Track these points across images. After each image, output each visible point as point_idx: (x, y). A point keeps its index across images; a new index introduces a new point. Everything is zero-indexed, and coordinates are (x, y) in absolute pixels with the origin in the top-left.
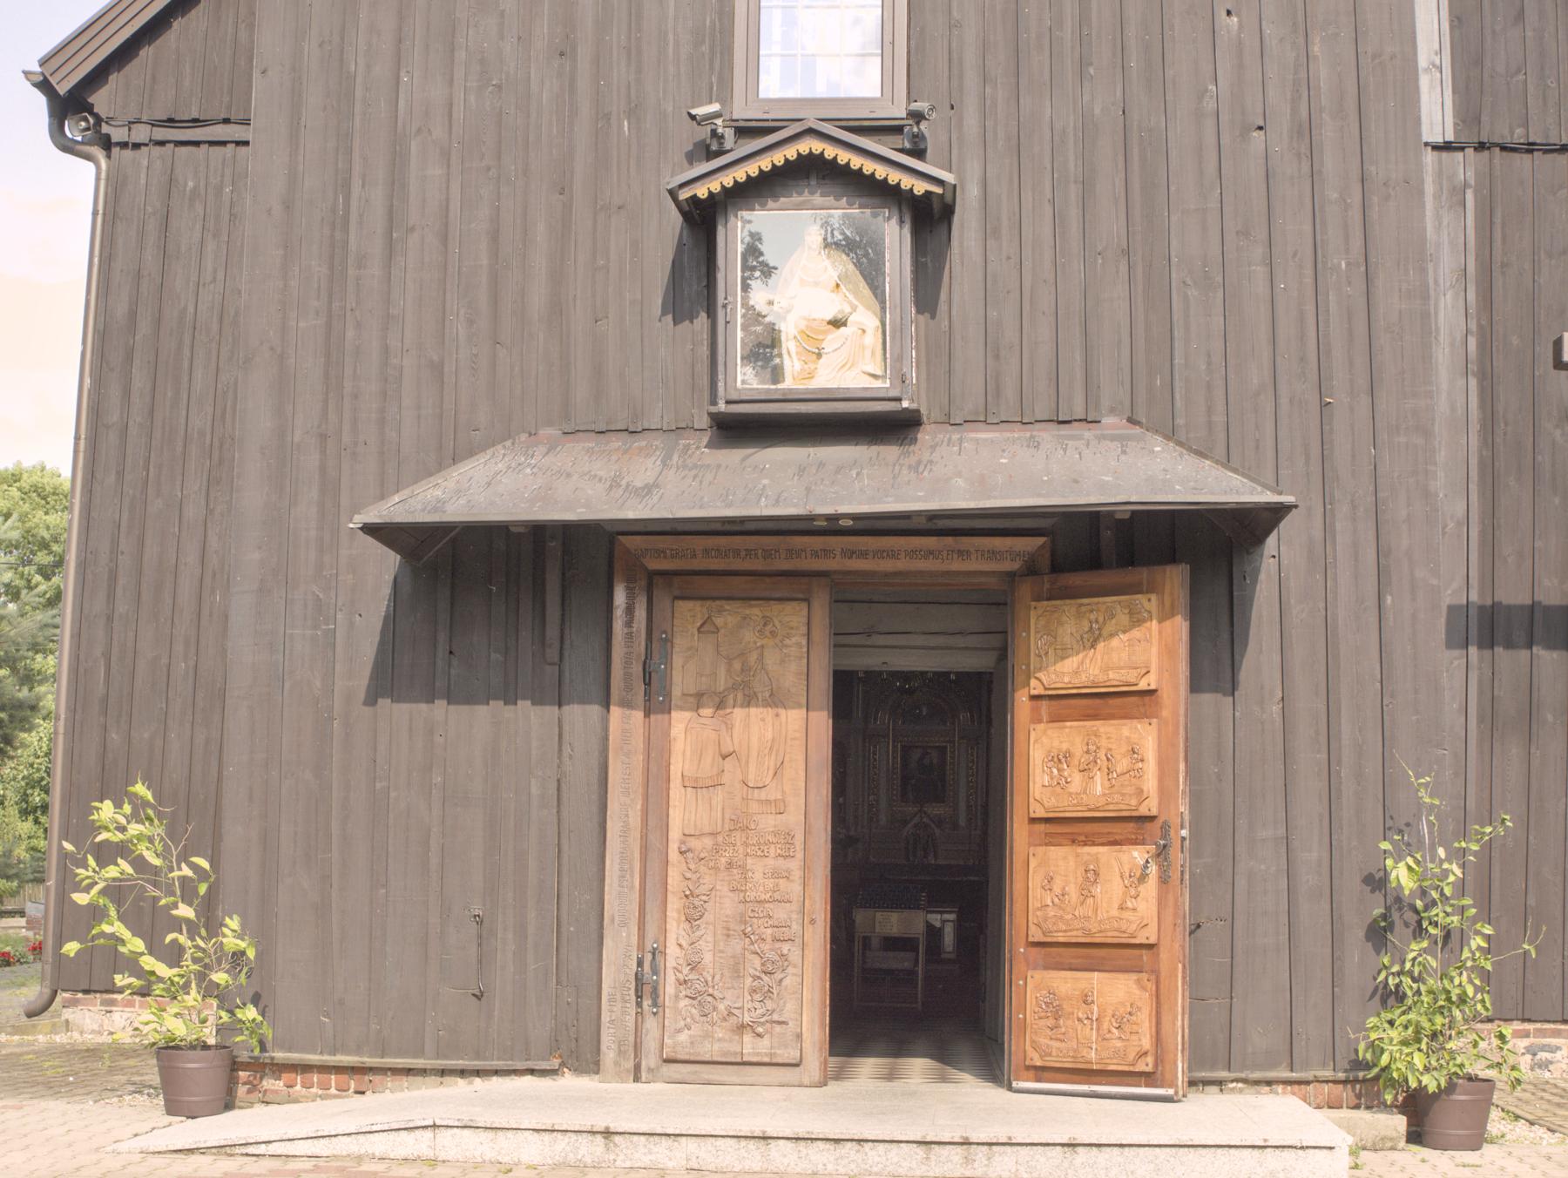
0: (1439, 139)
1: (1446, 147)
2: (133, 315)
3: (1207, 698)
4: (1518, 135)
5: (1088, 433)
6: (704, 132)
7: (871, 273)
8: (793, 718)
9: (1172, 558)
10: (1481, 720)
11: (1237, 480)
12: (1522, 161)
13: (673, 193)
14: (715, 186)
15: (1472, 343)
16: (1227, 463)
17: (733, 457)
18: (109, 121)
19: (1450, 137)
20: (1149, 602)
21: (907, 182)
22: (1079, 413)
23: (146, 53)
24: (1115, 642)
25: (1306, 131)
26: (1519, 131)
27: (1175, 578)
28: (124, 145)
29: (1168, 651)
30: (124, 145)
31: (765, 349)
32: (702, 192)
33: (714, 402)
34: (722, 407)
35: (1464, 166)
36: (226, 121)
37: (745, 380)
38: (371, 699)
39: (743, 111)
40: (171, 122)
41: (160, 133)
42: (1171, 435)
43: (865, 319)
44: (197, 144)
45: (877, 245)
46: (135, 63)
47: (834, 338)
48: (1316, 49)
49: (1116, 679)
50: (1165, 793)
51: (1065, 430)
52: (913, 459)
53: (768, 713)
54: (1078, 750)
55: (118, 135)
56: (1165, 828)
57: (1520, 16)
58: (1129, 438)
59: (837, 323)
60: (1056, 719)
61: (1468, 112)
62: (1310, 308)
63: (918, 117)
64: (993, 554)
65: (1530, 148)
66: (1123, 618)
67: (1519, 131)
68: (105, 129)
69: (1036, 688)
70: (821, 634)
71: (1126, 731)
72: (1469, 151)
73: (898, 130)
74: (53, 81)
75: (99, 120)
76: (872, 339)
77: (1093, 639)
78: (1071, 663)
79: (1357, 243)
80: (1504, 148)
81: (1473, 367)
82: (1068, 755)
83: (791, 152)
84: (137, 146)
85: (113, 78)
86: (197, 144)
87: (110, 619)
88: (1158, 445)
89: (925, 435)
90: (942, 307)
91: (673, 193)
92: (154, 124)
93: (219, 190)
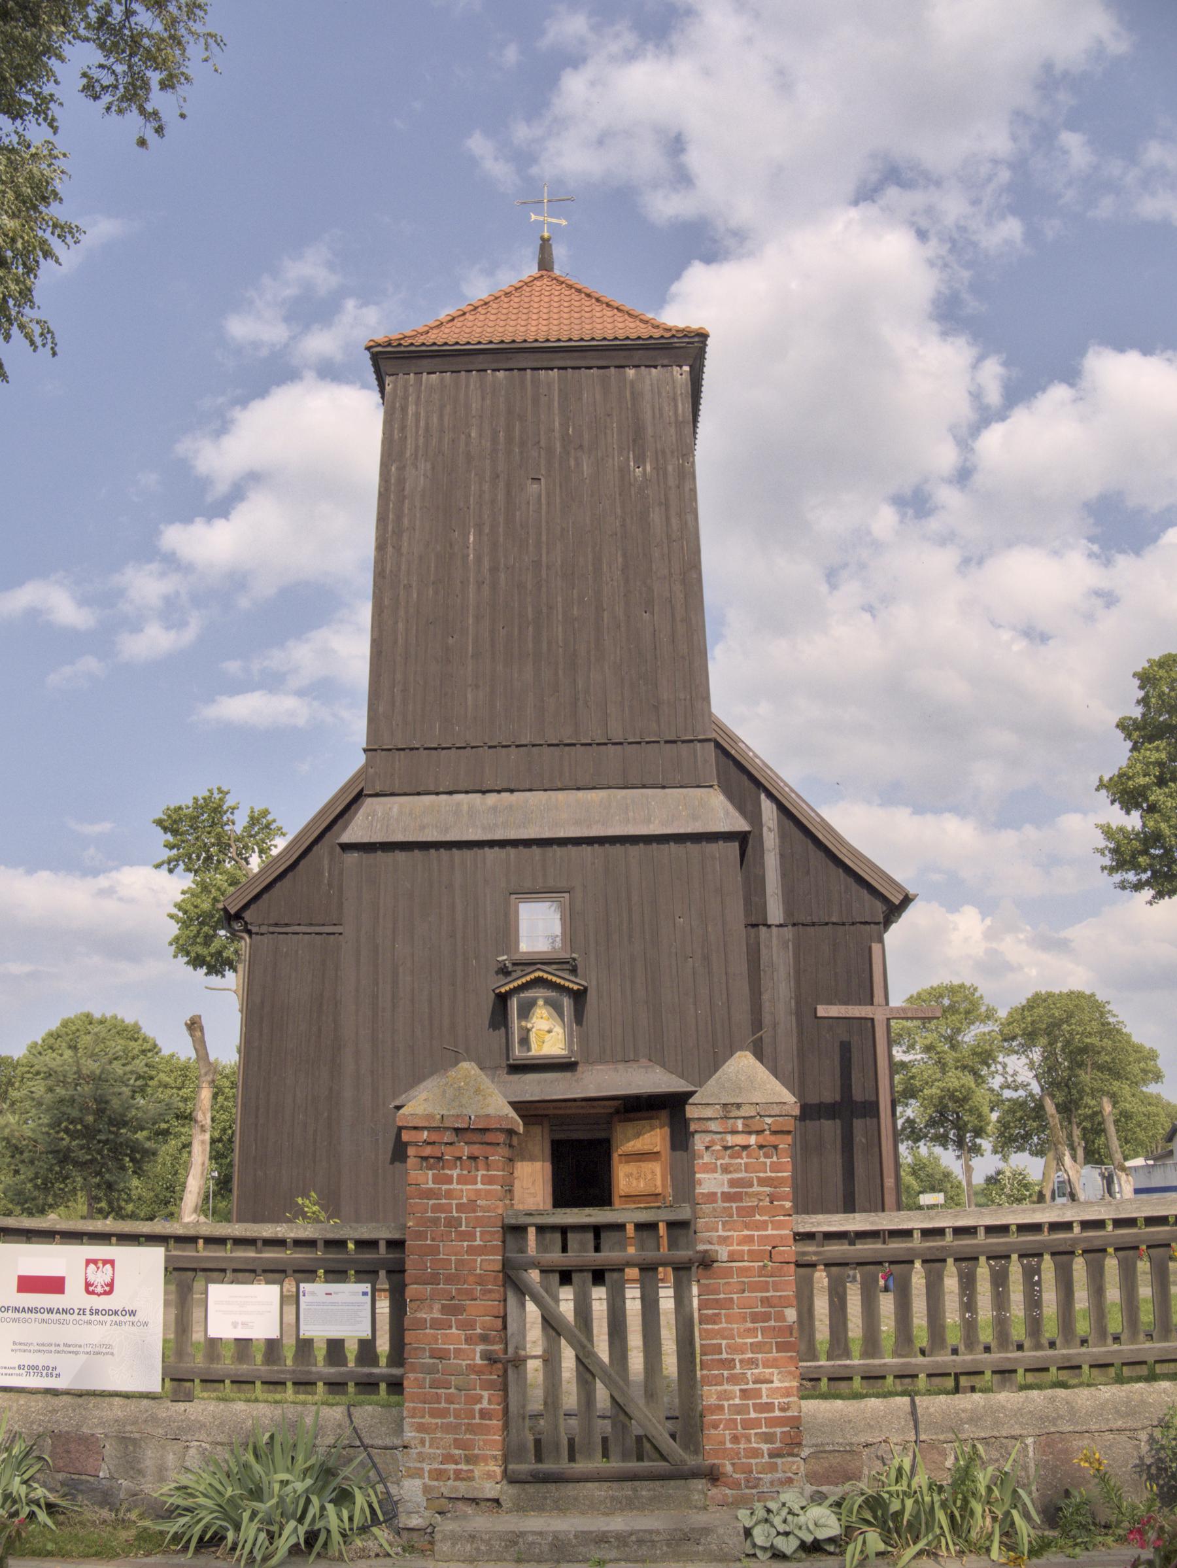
0: (778, 923)
1: (781, 926)
2: (262, 1002)
3: (678, 1153)
4: (808, 920)
5: (635, 1065)
6: (501, 965)
7: (561, 1015)
8: (538, 1165)
9: (664, 1108)
10: (801, 1149)
11: (683, 1082)
12: (811, 929)
13: (493, 991)
14: (507, 988)
15: (793, 1002)
16: (682, 1076)
17: (515, 1077)
18: (251, 924)
19: (782, 922)
20: (656, 1122)
21: (571, 985)
22: (632, 1057)
23: (266, 896)
24: (646, 1136)
25: (706, 958)
26: (809, 918)
27: (664, 1115)
28: (257, 934)
29: (663, 1139)
30: (257, 934)
31: (525, 1041)
32: (503, 990)
33: (508, 1059)
34: (511, 1062)
35: (788, 932)
36: (299, 925)
37: (517, 1052)
38: (392, 1162)
39: (516, 957)
40: (276, 925)
41: (272, 929)
42: (663, 1066)
43: (559, 1030)
44: (287, 933)
45: (562, 1006)
46: (261, 900)
47: (548, 1037)
48: (710, 929)
49: (647, 1148)
50: (664, 1186)
51: (628, 1064)
52: (576, 1078)
53: (529, 1163)
54: (635, 1172)
55: (254, 929)
56: (664, 1197)
57: (808, 873)
58: (648, 1067)
59: (549, 1031)
60: (627, 1162)
61: (789, 911)
62: (709, 1019)
63: (574, 959)
64: (604, 1107)
65: (813, 924)
66: (648, 1128)
67: (809, 918)
68: (249, 927)
69: (620, 1152)
70: (546, 1131)
71: (650, 1166)
72: (790, 927)
73: (568, 962)
74: (229, 908)
75: (246, 923)
76: (561, 1036)
77: (638, 1135)
78: (631, 1143)
79: (725, 996)
80: (803, 925)
81: (794, 1011)
82: (631, 1174)
83: (532, 976)
84: (262, 934)
85: (252, 906)
86: (287, 933)
87: (256, 1125)
88: (658, 1070)
89: (580, 1068)
90: (584, 1023)
91: (493, 991)
92: (270, 925)
93: (297, 951)
